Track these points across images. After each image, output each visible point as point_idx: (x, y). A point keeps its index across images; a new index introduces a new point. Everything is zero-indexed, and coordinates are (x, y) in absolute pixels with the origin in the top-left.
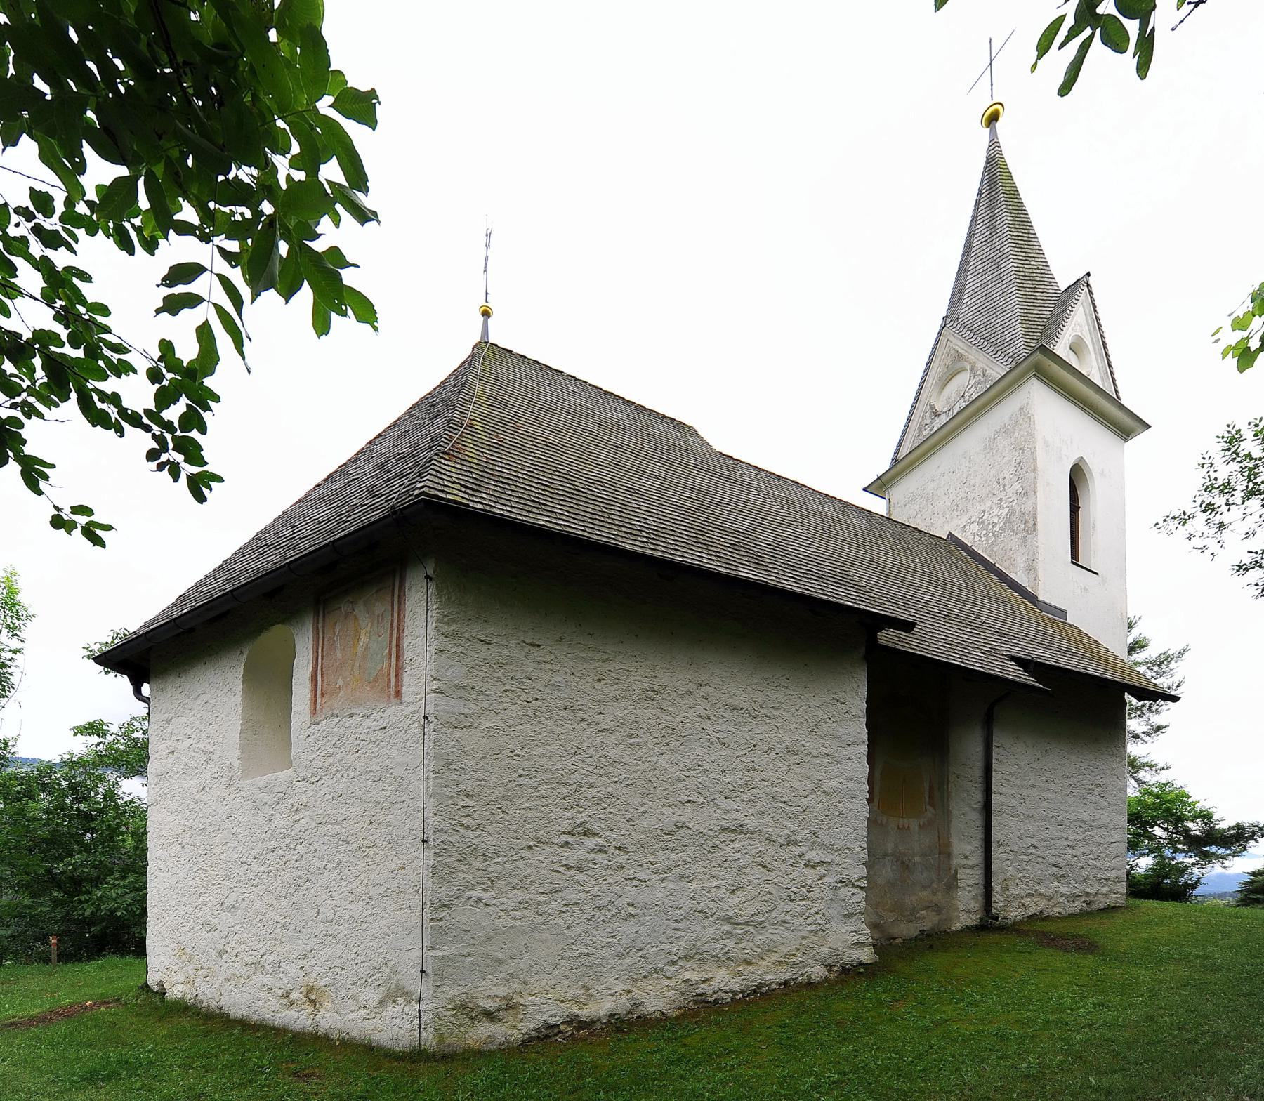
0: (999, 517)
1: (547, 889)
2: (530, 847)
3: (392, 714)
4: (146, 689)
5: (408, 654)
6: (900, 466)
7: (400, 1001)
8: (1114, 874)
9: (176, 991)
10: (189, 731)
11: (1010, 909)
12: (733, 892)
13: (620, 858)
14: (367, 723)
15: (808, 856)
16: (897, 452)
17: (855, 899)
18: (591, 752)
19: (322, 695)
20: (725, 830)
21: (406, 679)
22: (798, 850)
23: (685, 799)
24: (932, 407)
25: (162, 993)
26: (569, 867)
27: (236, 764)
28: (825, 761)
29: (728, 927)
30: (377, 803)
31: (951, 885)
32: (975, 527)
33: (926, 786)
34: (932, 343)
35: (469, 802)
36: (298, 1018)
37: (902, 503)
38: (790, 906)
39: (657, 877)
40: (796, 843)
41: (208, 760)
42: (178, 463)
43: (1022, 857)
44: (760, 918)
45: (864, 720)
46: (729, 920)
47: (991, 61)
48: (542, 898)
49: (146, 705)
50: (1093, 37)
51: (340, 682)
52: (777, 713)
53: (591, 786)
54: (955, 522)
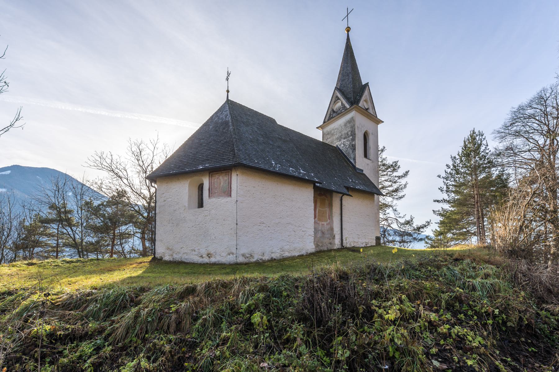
0: (348, 144)
3: (229, 199)
5: (233, 188)
6: (325, 124)
7: (231, 255)
8: (373, 237)
9: (167, 258)
10: (171, 197)
13: (269, 228)
14: (223, 200)
15: (303, 229)
16: (325, 119)
17: (312, 239)
18: (264, 208)
19: (212, 193)
20: (287, 223)
22: (301, 228)
23: (280, 217)
24: (333, 110)
26: (260, 230)
27: (187, 206)
28: (306, 210)
29: (288, 243)
31: (334, 237)
32: (342, 145)
33: (328, 215)
35: (244, 217)
36: (206, 260)
37: (326, 134)
40: (300, 227)
42: (335, 244)
44: (293, 242)
46: (288, 242)
54: (338, 143)
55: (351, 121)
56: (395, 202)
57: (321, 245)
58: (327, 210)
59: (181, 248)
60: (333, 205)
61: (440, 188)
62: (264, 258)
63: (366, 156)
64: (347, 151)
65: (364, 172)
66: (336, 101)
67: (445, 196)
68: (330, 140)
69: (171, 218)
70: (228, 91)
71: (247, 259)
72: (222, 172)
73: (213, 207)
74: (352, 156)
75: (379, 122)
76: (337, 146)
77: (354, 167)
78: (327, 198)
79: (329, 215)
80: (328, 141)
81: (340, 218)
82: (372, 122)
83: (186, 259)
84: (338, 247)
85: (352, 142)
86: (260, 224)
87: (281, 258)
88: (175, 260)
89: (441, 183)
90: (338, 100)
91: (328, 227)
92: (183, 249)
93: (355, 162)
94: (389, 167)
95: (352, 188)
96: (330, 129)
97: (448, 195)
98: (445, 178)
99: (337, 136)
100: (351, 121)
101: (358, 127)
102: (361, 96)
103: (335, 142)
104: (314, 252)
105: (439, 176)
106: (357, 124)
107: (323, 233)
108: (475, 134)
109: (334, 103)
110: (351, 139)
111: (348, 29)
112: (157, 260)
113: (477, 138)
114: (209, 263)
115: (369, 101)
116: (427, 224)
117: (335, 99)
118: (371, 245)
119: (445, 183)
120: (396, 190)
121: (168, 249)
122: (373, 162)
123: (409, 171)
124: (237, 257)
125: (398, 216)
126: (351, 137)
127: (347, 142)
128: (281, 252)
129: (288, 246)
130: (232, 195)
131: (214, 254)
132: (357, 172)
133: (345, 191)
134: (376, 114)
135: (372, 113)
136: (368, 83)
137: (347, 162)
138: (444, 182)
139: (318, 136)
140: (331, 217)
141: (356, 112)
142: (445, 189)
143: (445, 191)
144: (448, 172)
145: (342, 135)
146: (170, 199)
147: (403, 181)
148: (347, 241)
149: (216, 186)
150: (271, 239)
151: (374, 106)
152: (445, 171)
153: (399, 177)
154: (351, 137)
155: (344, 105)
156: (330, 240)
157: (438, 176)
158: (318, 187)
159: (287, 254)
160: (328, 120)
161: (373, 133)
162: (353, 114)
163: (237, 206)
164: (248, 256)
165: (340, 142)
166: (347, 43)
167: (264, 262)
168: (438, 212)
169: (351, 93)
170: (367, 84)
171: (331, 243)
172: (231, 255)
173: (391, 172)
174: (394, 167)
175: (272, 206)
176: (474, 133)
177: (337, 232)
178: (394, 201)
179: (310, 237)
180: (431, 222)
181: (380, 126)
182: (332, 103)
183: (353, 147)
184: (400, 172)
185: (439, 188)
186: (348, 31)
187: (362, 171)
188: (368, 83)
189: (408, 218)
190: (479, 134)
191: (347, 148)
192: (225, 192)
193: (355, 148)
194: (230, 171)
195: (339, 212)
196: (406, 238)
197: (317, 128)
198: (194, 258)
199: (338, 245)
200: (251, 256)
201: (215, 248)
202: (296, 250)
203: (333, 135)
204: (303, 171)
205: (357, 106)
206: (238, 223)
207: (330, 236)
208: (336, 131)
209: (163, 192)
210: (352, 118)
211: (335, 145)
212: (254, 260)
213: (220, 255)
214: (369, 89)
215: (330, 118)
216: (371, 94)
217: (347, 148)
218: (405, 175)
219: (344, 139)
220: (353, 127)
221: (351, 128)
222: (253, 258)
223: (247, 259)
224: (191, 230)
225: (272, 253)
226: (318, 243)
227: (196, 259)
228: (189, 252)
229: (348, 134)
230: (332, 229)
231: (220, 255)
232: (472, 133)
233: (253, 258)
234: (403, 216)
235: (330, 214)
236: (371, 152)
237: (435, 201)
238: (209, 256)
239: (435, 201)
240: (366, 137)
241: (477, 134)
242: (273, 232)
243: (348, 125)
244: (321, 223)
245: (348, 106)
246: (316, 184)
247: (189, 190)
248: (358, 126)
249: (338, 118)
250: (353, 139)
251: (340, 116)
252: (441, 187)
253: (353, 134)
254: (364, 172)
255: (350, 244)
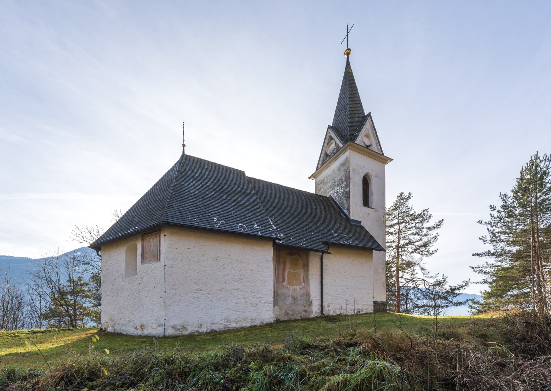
0: (341, 192)
1: (192, 302)
2: (188, 293)
3: (158, 264)
4: (100, 253)
6: (318, 171)
7: (161, 326)
8: (369, 303)
9: (110, 330)
10: (112, 265)
11: (326, 313)
12: (237, 304)
14: (153, 266)
15: (256, 296)
21: (161, 257)
22: (254, 294)
24: (326, 154)
25: (105, 330)
27: (124, 273)
29: (235, 312)
30: (156, 283)
31: (311, 304)
32: (336, 194)
33: (302, 278)
34: (326, 133)
35: (174, 283)
36: (140, 332)
37: (319, 183)
38: (251, 308)
39: (218, 300)
40: (253, 293)
41: (117, 272)
43: (334, 297)
44: (243, 310)
45: (272, 262)
47: (348, 34)
48: (191, 304)
49: (100, 257)
50: (349, 64)
51: (147, 256)
52: (248, 261)
53: (202, 279)
54: (331, 192)
55: (345, 163)
56: (425, 259)
57: (291, 313)
58: (301, 272)
59: (121, 319)
60: (310, 265)
61: (481, 237)
62: (200, 330)
63: (366, 202)
64: (340, 200)
65: (362, 224)
66: (330, 141)
67: (490, 247)
68: (323, 190)
69: (112, 288)
70: (184, 146)
71: (178, 332)
72: (153, 233)
73: (145, 274)
74: (346, 206)
75: (385, 160)
76: (330, 196)
77: (348, 218)
78: (301, 257)
79: (303, 278)
80: (321, 191)
81: (319, 280)
82: (376, 161)
83: (124, 331)
84: (316, 315)
85: (346, 189)
86: (196, 291)
87: (226, 329)
88: (115, 332)
89: (484, 231)
90: (331, 140)
91: (303, 291)
92: (122, 320)
93: (349, 213)
94: (417, 218)
95: (334, 243)
96: (323, 177)
97: (494, 245)
98: (489, 224)
99: (330, 184)
100: (345, 163)
101: (354, 170)
102: (359, 131)
103: (328, 191)
104: (272, 322)
105: (480, 222)
106: (352, 165)
107: (295, 299)
108: (538, 160)
109: (328, 144)
110: (345, 185)
111: (348, 52)
112: (349, 318)
113: (542, 165)
114: (142, 335)
115: (372, 136)
116: (464, 284)
117: (328, 140)
118: (366, 312)
119: (489, 231)
120: (425, 245)
121: (110, 320)
122: (376, 211)
123: (443, 220)
124: (166, 329)
125: (427, 276)
126: (345, 183)
127: (341, 190)
128: (226, 323)
129: (236, 316)
130: (161, 259)
131: (146, 325)
132: (351, 225)
133: (324, 248)
134: (382, 151)
135: (376, 151)
136: (370, 113)
137: (339, 213)
138: (488, 229)
139: (310, 187)
140: (306, 279)
141: (353, 152)
142: (489, 238)
143: (488, 241)
144: (496, 216)
145: (335, 183)
146: (112, 268)
147: (433, 233)
148: (330, 308)
149: (147, 250)
150: (211, 307)
151: (379, 141)
152: (491, 215)
153: (429, 229)
154: (345, 183)
155: (338, 145)
156: (304, 307)
157: (479, 222)
158: (278, 244)
159: (234, 325)
160: (322, 166)
161: (378, 175)
162: (348, 154)
163: (166, 271)
164: (180, 328)
165: (334, 191)
166: (346, 68)
167: (200, 334)
168: (477, 269)
169: (347, 130)
170: (369, 115)
171: (305, 311)
172: (161, 326)
173: (420, 223)
174: (424, 217)
175: (213, 270)
176: (537, 158)
177: (315, 297)
178: (423, 258)
179: (267, 304)
180: (470, 282)
181: (388, 167)
182: (325, 145)
183: (347, 194)
184: (432, 223)
185: (480, 238)
186: (348, 54)
187: (360, 222)
188: (370, 113)
189: (440, 278)
190: (546, 159)
191: (341, 197)
192: (154, 257)
193: (349, 195)
194: (159, 232)
195: (319, 273)
196: (439, 302)
197: (309, 178)
198: (130, 330)
199: (316, 313)
200: (184, 328)
201: (147, 319)
202: (248, 320)
203: (326, 183)
204: (258, 226)
205: (352, 143)
206: (166, 290)
207: (304, 302)
208: (329, 178)
209: (106, 261)
210: (346, 159)
211: (328, 196)
212: (187, 332)
213: (151, 327)
214: (372, 121)
215: (323, 163)
216: (374, 126)
217: (341, 197)
218: (439, 225)
219: (337, 186)
220: (347, 171)
221: (345, 172)
222: (186, 330)
223: (178, 332)
224: (128, 300)
225: (213, 324)
226: (287, 311)
227: (131, 331)
228: (126, 323)
229: (341, 180)
230: (308, 294)
231: (151, 327)
232: (533, 158)
233: (186, 330)
234: (434, 276)
235: (305, 277)
236: (374, 199)
237: (474, 255)
238: (142, 327)
239: (474, 255)
240: (366, 181)
241: (541, 158)
242: (214, 300)
243: (342, 169)
244: (291, 287)
245: (341, 145)
246: (277, 241)
247: (126, 256)
248: (355, 168)
249: (331, 161)
250: (348, 185)
251: (334, 159)
252: (482, 237)
253: (348, 179)
254: (362, 224)
255: (334, 312)
